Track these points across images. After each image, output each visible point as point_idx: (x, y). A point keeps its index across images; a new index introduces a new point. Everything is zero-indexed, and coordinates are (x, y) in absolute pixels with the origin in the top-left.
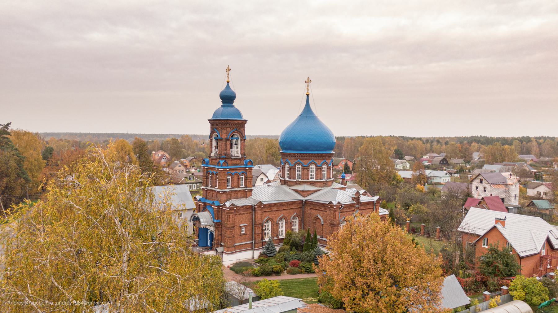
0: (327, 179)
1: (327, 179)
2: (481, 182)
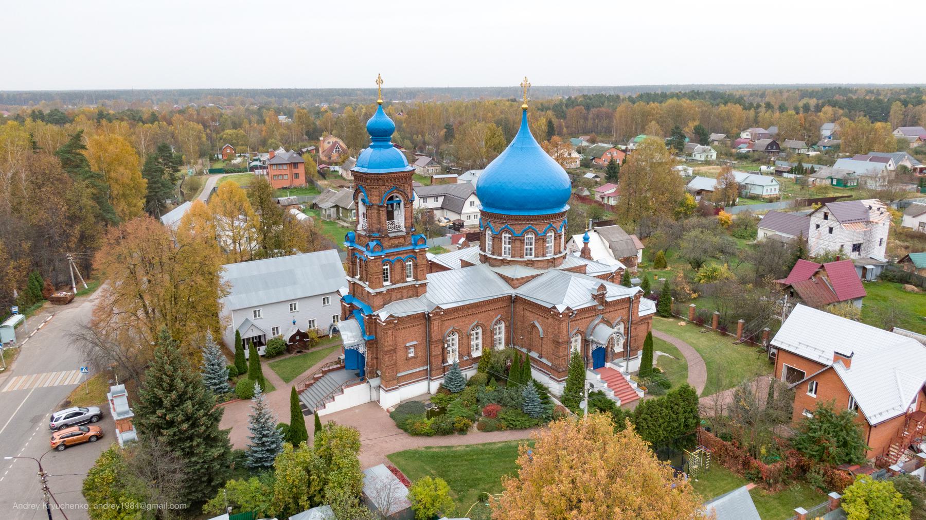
0: (555, 254)
1: (555, 254)
2: (826, 217)
